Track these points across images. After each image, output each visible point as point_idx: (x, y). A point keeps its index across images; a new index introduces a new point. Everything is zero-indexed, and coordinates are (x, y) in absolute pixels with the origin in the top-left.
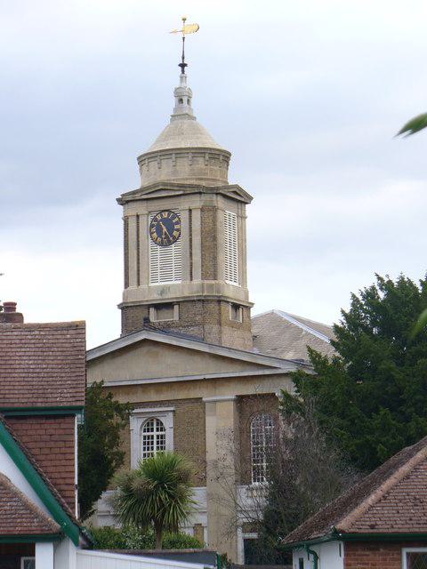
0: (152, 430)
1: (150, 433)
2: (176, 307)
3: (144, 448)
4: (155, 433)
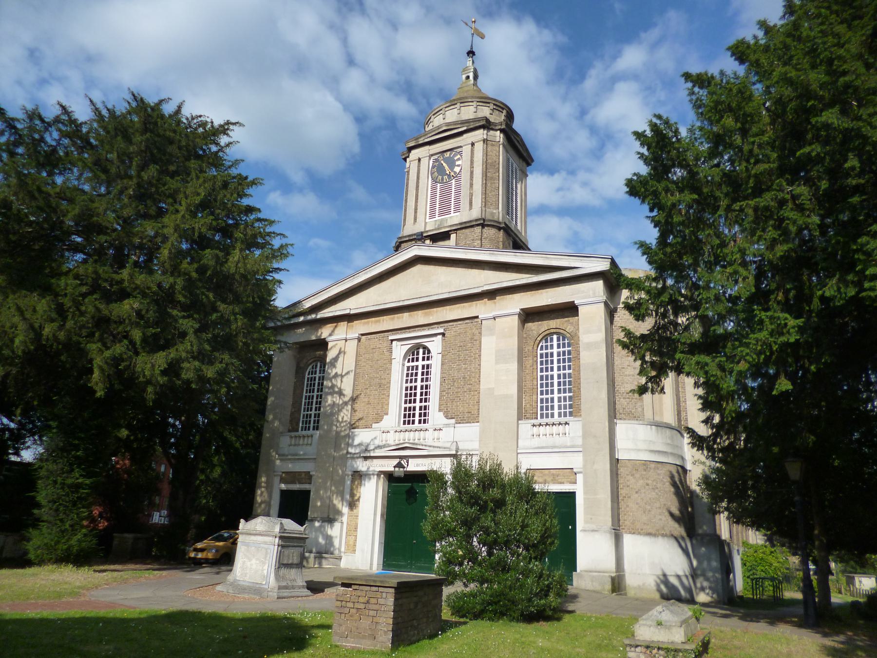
0: (417, 360)
1: (412, 405)
2: (453, 236)
3: (404, 422)
4: (420, 363)
